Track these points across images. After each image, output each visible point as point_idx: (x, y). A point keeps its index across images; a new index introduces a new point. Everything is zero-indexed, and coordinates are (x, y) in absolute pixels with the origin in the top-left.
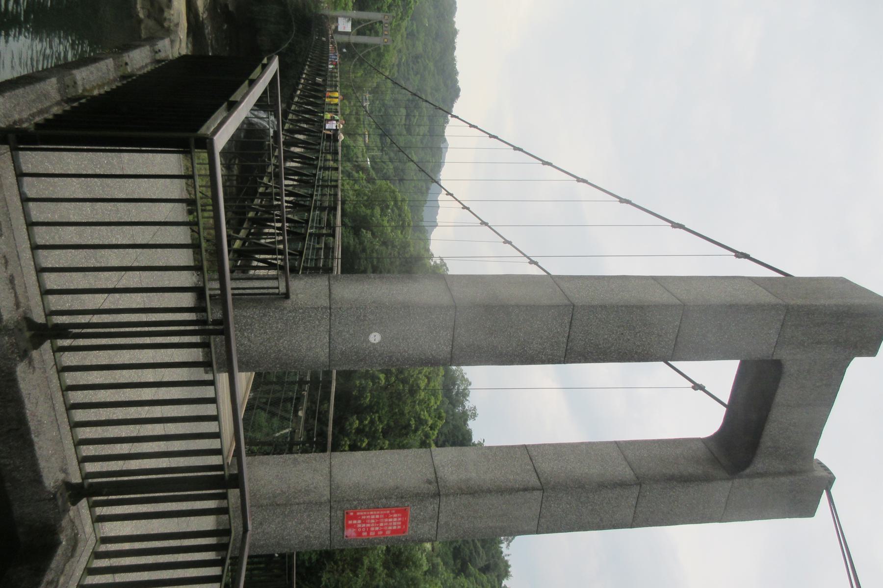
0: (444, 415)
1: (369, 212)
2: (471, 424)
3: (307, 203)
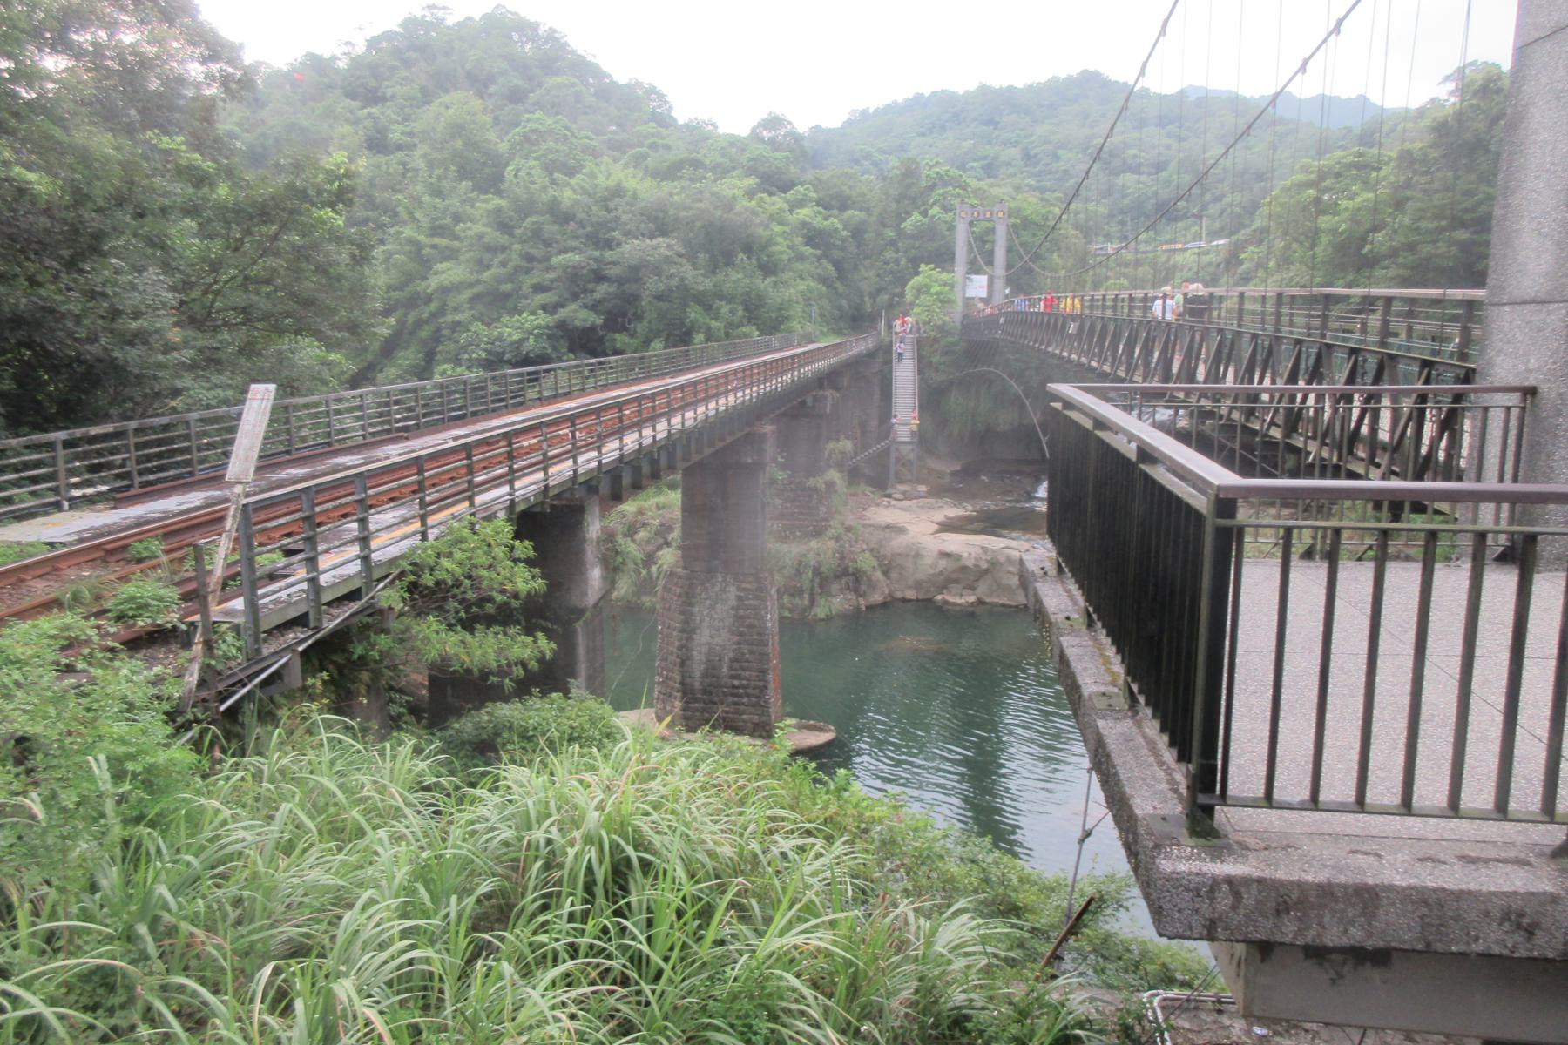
1: (1325, 239)
3: (1314, 351)
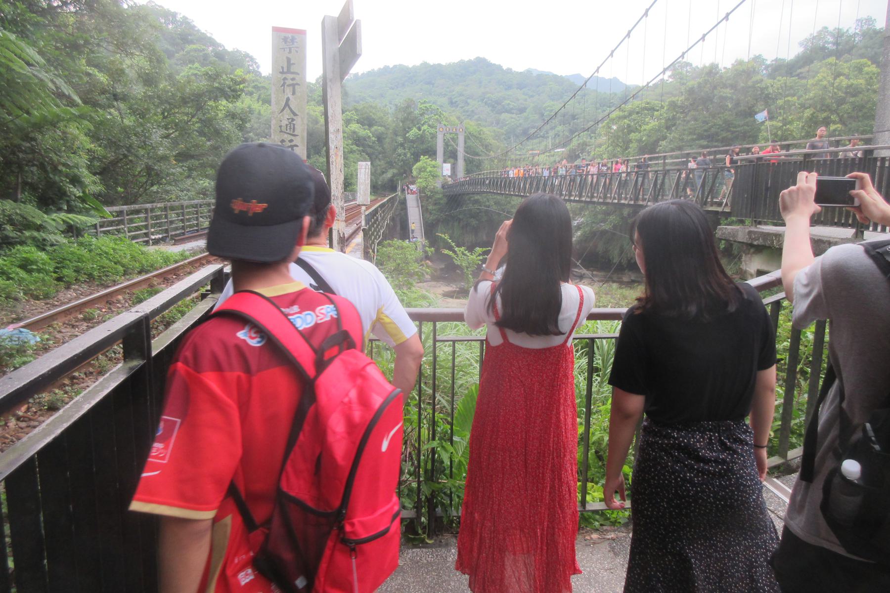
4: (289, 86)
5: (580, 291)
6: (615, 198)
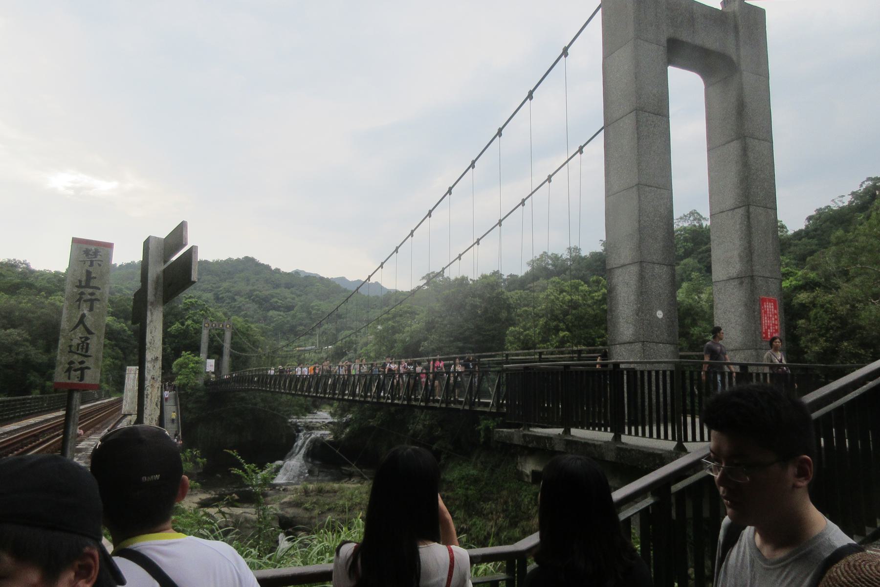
0: (595, 278)
2: (585, 253)
4: (85, 301)
5: (451, 551)
6: (388, 398)
